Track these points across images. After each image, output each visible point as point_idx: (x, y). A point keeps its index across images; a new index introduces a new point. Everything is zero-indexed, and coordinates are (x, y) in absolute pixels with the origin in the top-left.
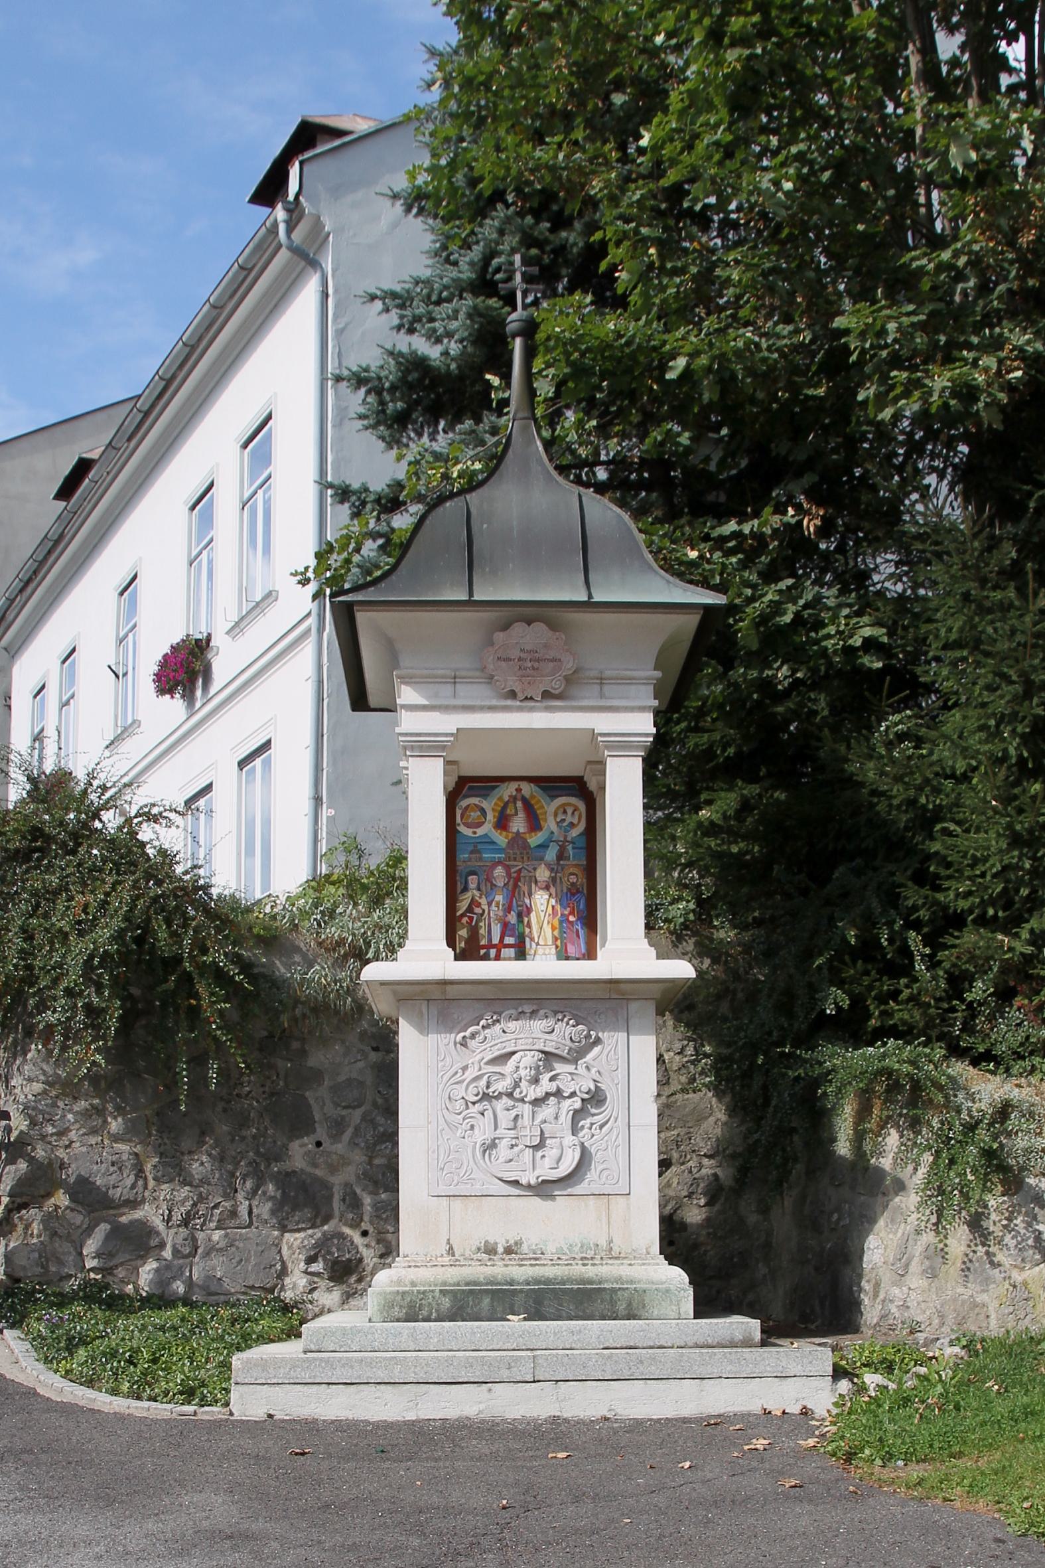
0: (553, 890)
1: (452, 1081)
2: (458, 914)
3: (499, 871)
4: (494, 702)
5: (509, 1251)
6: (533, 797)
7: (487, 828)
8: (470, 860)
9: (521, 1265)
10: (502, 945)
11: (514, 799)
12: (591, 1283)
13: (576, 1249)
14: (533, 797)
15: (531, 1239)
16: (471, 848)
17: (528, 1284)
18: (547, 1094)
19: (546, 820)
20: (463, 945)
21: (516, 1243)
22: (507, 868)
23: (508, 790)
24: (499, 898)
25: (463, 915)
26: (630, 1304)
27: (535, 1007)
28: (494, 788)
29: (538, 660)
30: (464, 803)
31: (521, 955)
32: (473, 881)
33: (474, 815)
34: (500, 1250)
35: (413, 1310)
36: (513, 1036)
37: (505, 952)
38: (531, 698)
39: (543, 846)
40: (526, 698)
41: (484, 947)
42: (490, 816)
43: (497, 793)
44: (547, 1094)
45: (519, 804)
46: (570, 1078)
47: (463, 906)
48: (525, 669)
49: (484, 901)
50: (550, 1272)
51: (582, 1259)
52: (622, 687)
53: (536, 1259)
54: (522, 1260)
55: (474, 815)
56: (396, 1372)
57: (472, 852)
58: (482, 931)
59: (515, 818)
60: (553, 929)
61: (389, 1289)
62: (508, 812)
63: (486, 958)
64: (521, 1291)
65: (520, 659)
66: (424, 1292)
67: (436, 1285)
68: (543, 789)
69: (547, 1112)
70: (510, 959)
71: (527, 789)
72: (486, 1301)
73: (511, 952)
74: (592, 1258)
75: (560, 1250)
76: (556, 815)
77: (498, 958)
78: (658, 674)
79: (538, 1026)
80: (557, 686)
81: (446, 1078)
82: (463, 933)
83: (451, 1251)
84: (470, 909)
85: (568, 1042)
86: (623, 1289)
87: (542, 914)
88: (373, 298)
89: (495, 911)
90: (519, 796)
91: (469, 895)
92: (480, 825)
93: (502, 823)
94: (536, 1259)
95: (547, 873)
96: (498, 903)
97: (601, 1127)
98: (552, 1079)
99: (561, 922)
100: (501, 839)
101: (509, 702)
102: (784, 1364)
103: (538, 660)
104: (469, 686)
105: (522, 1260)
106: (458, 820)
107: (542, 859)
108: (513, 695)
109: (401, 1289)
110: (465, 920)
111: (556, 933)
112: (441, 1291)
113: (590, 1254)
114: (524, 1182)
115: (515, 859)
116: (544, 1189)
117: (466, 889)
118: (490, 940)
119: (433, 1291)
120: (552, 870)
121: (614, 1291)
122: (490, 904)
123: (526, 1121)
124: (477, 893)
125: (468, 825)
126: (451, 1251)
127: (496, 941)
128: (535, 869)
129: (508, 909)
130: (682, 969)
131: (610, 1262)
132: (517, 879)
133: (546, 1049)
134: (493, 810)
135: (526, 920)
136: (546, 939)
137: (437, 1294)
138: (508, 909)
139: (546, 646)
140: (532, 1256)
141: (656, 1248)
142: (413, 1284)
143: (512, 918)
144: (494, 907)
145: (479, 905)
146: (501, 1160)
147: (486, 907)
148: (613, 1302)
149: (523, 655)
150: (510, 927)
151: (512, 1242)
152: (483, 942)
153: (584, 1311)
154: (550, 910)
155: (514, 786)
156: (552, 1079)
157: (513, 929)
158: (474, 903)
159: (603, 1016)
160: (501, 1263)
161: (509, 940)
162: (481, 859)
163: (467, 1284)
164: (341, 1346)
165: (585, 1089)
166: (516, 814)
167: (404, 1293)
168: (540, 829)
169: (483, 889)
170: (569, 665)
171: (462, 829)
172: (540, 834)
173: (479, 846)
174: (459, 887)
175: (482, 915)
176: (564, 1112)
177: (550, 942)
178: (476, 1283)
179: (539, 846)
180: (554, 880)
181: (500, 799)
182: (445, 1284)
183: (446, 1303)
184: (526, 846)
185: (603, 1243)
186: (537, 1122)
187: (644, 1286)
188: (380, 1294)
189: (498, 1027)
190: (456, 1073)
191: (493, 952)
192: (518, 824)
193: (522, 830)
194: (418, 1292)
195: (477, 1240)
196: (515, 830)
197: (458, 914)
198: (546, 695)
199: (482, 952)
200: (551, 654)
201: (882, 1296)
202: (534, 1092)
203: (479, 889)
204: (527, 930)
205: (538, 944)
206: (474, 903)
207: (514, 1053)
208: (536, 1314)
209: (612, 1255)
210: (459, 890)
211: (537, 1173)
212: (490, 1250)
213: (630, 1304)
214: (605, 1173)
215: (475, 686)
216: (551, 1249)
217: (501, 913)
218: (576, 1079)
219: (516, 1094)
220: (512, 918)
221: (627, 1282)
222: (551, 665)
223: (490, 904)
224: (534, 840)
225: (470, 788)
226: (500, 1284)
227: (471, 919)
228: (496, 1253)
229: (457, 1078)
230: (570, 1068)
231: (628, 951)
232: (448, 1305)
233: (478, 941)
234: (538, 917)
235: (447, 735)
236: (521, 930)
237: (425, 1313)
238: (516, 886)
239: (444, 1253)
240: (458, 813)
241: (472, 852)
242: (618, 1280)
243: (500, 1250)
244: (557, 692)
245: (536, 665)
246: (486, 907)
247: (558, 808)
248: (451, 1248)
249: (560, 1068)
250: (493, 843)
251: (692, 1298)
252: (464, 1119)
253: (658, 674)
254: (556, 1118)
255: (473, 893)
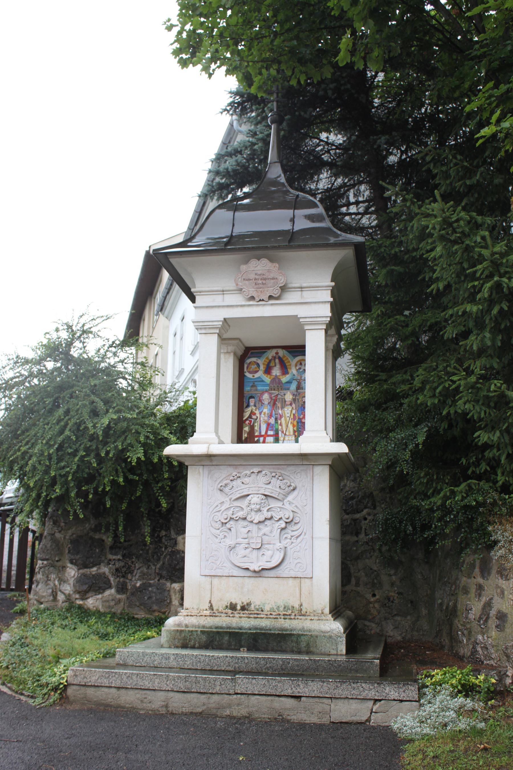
0: (294, 405)
1: (215, 511)
2: (244, 419)
3: (266, 396)
4: (244, 303)
5: (243, 608)
6: (284, 356)
7: (260, 374)
8: (251, 390)
9: (249, 618)
10: (267, 435)
11: (274, 358)
12: (287, 630)
13: (281, 609)
14: (284, 356)
15: (257, 601)
16: (251, 384)
17: (250, 629)
18: (266, 519)
19: (291, 368)
20: (246, 435)
21: (248, 604)
22: (270, 394)
23: (271, 354)
24: (266, 410)
25: (247, 420)
26: (308, 645)
27: (260, 470)
28: (265, 352)
29: (265, 279)
30: (248, 361)
31: (277, 440)
32: (252, 402)
33: (254, 367)
34: (239, 607)
35: (185, 640)
36: (247, 486)
37: (268, 439)
38: (263, 300)
39: (289, 382)
40: (260, 300)
41: (257, 436)
42: (262, 368)
43: (265, 355)
44: (266, 519)
45: (277, 361)
46: (279, 509)
47: (246, 415)
48: (259, 284)
49: (257, 412)
50: (264, 623)
51: (284, 615)
52: (313, 292)
53: (258, 614)
54: (251, 614)
55: (254, 367)
56: (156, 683)
57: (252, 386)
58: (256, 428)
59: (275, 368)
60: (294, 426)
61: (173, 628)
62: (271, 365)
63: (258, 442)
64: (246, 633)
65: (255, 279)
66: (192, 631)
67: (199, 627)
68: (289, 352)
69: (265, 529)
70: (270, 443)
71: (282, 353)
72: (226, 638)
73: (271, 439)
74: (290, 615)
75: (272, 610)
76: (296, 366)
77: (264, 442)
78: (333, 284)
79: (262, 479)
80: (276, 292)
81: (211, 509)
82: (246, 429)
83: (211, 607)
84: (250, 417)
85: (278, 490)
86: (305, 635)
87: (288, 419)
88: (222, 113)
89: (263, 418)
90: (277, 357)
91: (250, 409)
92: (256, 372)
93: (268, 371)
94: (258, 614)
95: (291, 397)
96: (265, 413)
97: (297, 537)
98: (268, 510)
99: (298, 422)
100: (267, 379)
101: (251, 303)
102: (387, 691)
103: (265, 279)
104: (231, 295)
105: (251, 614)
106: (245, 370)
107: (288, 389)
108: (252, 298)
109: (179, 629)
110: (247, 422)
111: (295, 429)
112: (201, 631)
113: (290, 612)
114: (251, 568)
115: (274, 390)
116: (259, 573)
117: (248, 406)
118: (260, 433)
119: (197, 631)
120: (294, 395)
121: (299, 636)
122: (260, 413)
123: (254, 533)
124: (254, 408)
125: (250, 372)
126: (211, 607)
127: (263, 433)
128: (285, 395)
129: (271, 416)
130: (342, 448)
131: (300, 617)
132: (275, 401)
133: (266, 493)
134: (264, 364)
135: (279, 422)
136: (290, 432)
137: (199, 633)
138: (271, 416)
139: (269, 271)
140: (256, 612)
141: (327, 610)
142: (187, 626)
143: (272, 421)
144: (262, 415)
145: (255, 414)
146: (240, 556)
147: (258, 415)
148: (297, 642)
149: (257, 277)
150: (271, 425)
151: (245, 603)
152: (257, 434)
153: (281, 647)
154: (292, 416)
155: (274, 351)
156: (268, 510)
157: (272, 427)
158: (252, 413)
159: (299, 474)
160: (237, 615)
161: (270, 433)
162: (257, 390)
163: (216, 628)
164: (137, 663)
165: (287, 516)
166: (275, 366)
167: (181, 631)
168: (288, 373)
169: (257, 405)
170: (282, 282)
171: (247, 374)
172: (287, 376)
173: (256, 383)
174: (245, 405)
175: (256, 419)
176: (276, 528)
177: (292, 433)
178: (221, 628)
179: (287, 382)
180: (294, 400)
181: (267, 358)
182: (204, 627)
183: (204, 638)
184: (280, 382)
185: (297, 606)
186: (260, 534)
187: (317, 633)
188: (167, 631)
189: (239, 481)
190: (217, 506)
191: (262, 439)
192: (276, 371)
193: (278, 374)
194: (189, 631)
195: (226, 602)
196: (274, 374)
197: (244, 419)
198: (271, 297)
199: (256, 439)
200: (272, 276)
201: (473, 640)
202: (258, 518)
203: (255, 406)
204: (280, 427)
205: (285, 435)
206: (252, 413)
207: (248, 495)
208: (253, 647)
209: (301, 613)
210: (245, 406)
211: (259, 564)
212: (233, 607)
213: (308, 645)
214: (299, 565)
215: (234, 295)
216: (267, 608)
217: (266, 418)
218: (282, 510)
219: (249, 518)
220: (272, 421)
221: (307, 631)
222: (272, 281)
223: (260, 413)
224: (284, 379)
225: (252, 353)
226: (235, 629)
227: (251, 421)
228: (236, 610)
229: (217, 509)
230: (280, 504)
231: (319, 437)
232: (205, 640)
233: (254, 433)
234: (285, 420)
235: (218, 321)
236: (277, 427)
237: (192, 643)
238: (274, 404)
239: (208, 608)
240: (246, 366)
241: (252, 386)
242: (303, 629)
243: (239, 607)
244: (277, 296)
245: (264, 282)
246: (258, 415)
247: (297, 362)
248: (211, 606)
249: (274, 504)
250: (263, 381)
251: (344, 642)
252: (221, 532)
253: (333, 284)
254: (271, 532)
255: (252, 408)
